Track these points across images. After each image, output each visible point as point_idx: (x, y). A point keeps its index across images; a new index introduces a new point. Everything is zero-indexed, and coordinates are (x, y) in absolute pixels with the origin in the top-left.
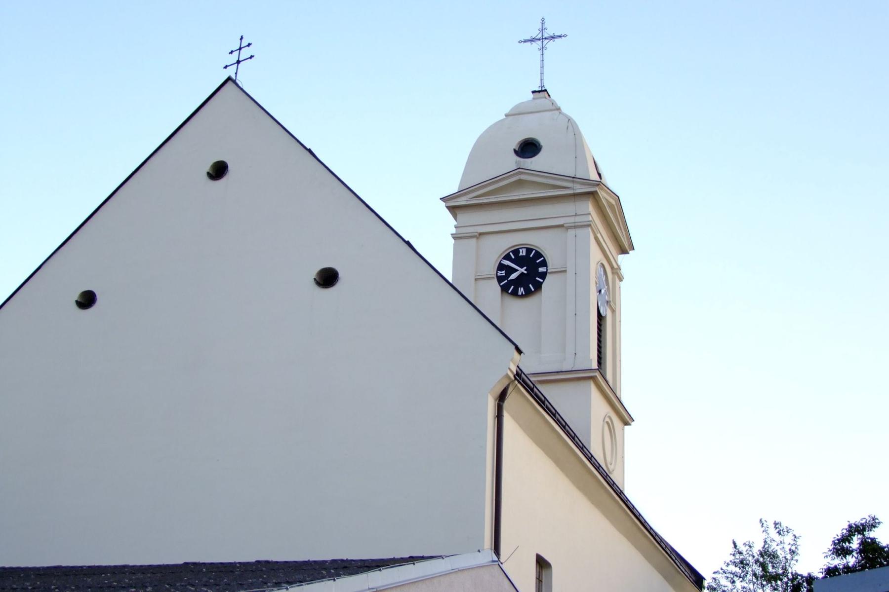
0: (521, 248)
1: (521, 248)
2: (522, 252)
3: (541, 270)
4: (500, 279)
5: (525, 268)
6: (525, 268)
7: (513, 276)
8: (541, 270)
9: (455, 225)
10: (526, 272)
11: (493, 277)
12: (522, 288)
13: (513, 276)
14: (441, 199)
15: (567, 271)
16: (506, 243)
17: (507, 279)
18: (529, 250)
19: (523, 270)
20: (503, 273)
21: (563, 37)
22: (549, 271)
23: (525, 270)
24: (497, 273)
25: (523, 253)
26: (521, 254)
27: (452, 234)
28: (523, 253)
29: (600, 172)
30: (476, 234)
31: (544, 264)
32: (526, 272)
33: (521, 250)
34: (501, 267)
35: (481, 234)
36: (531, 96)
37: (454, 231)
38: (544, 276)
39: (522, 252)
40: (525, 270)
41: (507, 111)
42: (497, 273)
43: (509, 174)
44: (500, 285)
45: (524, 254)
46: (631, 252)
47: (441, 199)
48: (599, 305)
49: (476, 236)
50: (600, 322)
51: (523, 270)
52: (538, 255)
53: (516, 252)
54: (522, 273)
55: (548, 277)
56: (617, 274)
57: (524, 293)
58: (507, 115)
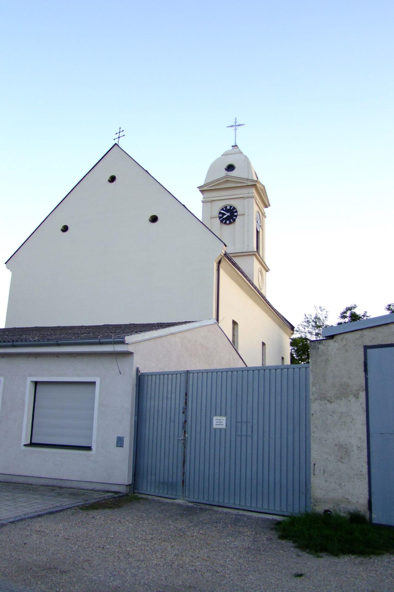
3: (235, 214)
4: (220, 218)
7: (225, 217)
8: (235, 214)
13: (225, 217)
18: (231, 207)
20: (221, 215)
22: (238, 214)
25: (228, 208)
26: (228, 208)
27: (198, 187)
31: (236, 212)
32: (229, 215)
34: (220, 213)
36: (231, 148)
37: (202, 200)
38: (236, 216)
45: (229, 208)
52: (234, 208)
53: (226, 207)
54: (228, 215)
55: (238, 217)
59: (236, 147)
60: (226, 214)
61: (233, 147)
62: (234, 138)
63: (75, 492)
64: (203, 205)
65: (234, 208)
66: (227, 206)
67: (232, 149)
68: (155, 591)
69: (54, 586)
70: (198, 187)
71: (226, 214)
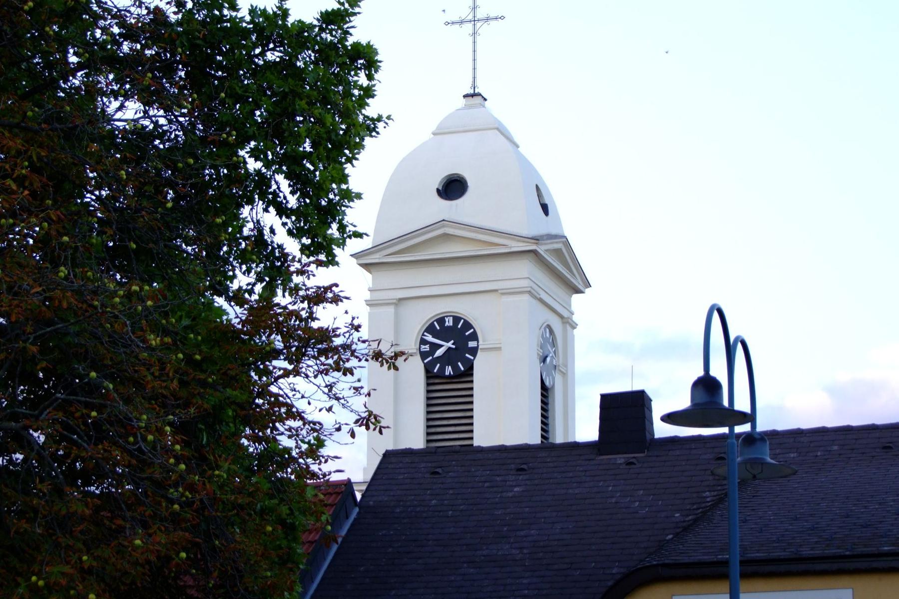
0: (447, 316)
1: (447, 316)
2: (449, 321)
3: (472, 344)
4: (424, 355)
5: (452, 341)
6: (452, 341)
7: (439, 353)
8: (472, 344)
9: (369, 288)
10: (454, 347)
11: (415, 353)
12: (450, 367)
13: (439, 353)
14: (351, 255)
15: (474, 396)
16: (428, 312)
17: (433, 355)
18: (456, 319)
19: (450, 344)
20: (426, 348)
21: (500, 19)
22: (480, 347)
23: (453, 344)
24: (420, 347)
25: (449, 322)
26: (447, 324)
27: (365, 301)
28: (449, 322)
29: (547, 202)
30: (395, 301)
31: (474, 337)
32: (454, 347)
33: (447, 319)
34: (423, 342)
35: (400, 300)
36: (463, 102)
37: (368, 296)
38: (474, 352)
39: (449, 321)
40: (453, 344)
41: (434, 128)
42: (420, 347)
43: (384, 245)
44: (423, 362)
45: (451, 324)
46: (587, 290)
47: (351, 255)
48: (544, 377)
49: (395, 303)
50: (545, 393)
51: (450, 344)
52: (468, 325)
53: (441, 321)
54: (450, 348)
55: (480, 354)
56: (568, 322)
57: (452, 373)
58: (434, 134)
59: (477, 100)
60: (441, 346)
61: (466, 98)
62: (478, 66)
63: (56, 413)
64: (369, 313)
65: (466, 322)
66: (444, 317)
67: (467, 107)
68: (92, 3)
69: (16, 313)
70: (365, 301)
71: (441, 346)
